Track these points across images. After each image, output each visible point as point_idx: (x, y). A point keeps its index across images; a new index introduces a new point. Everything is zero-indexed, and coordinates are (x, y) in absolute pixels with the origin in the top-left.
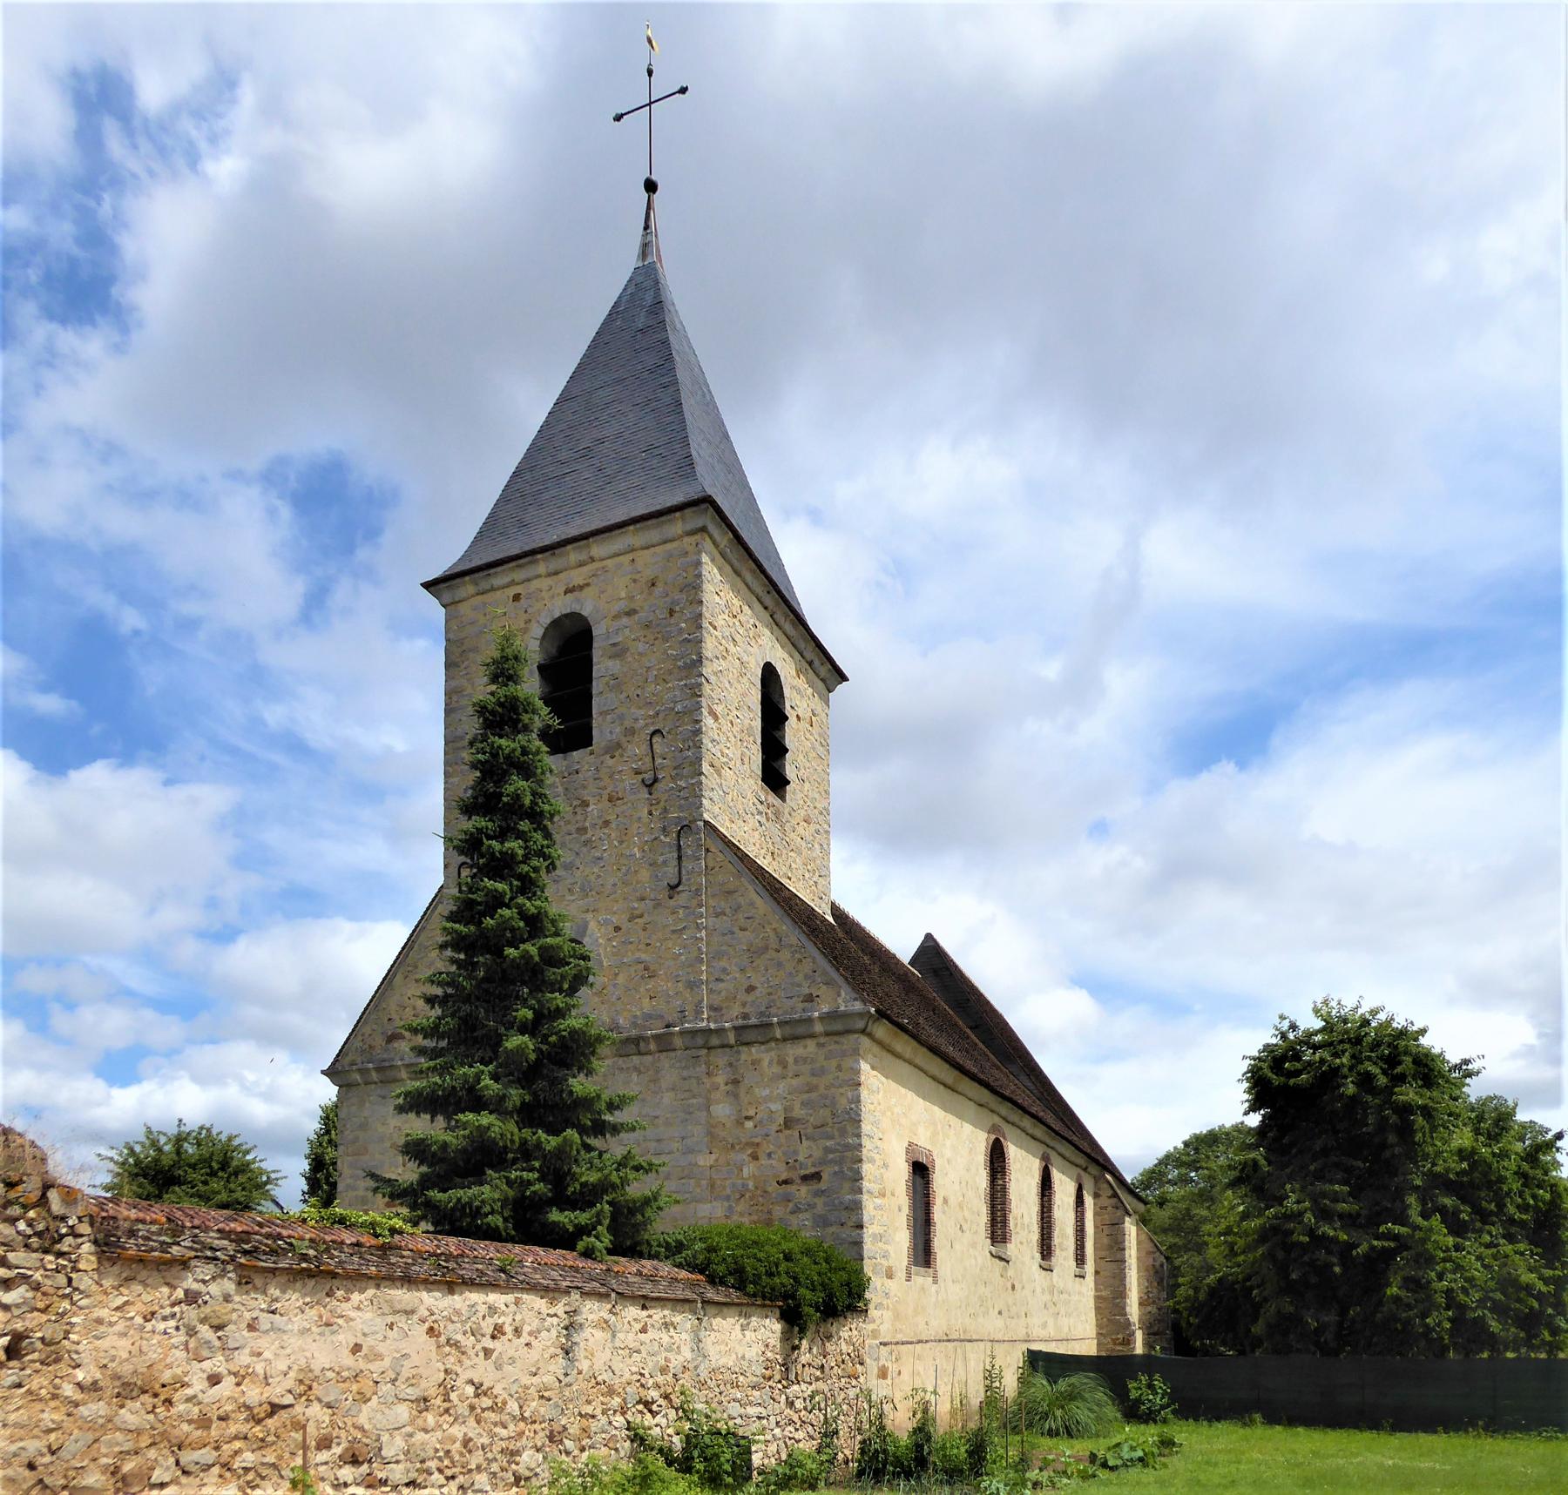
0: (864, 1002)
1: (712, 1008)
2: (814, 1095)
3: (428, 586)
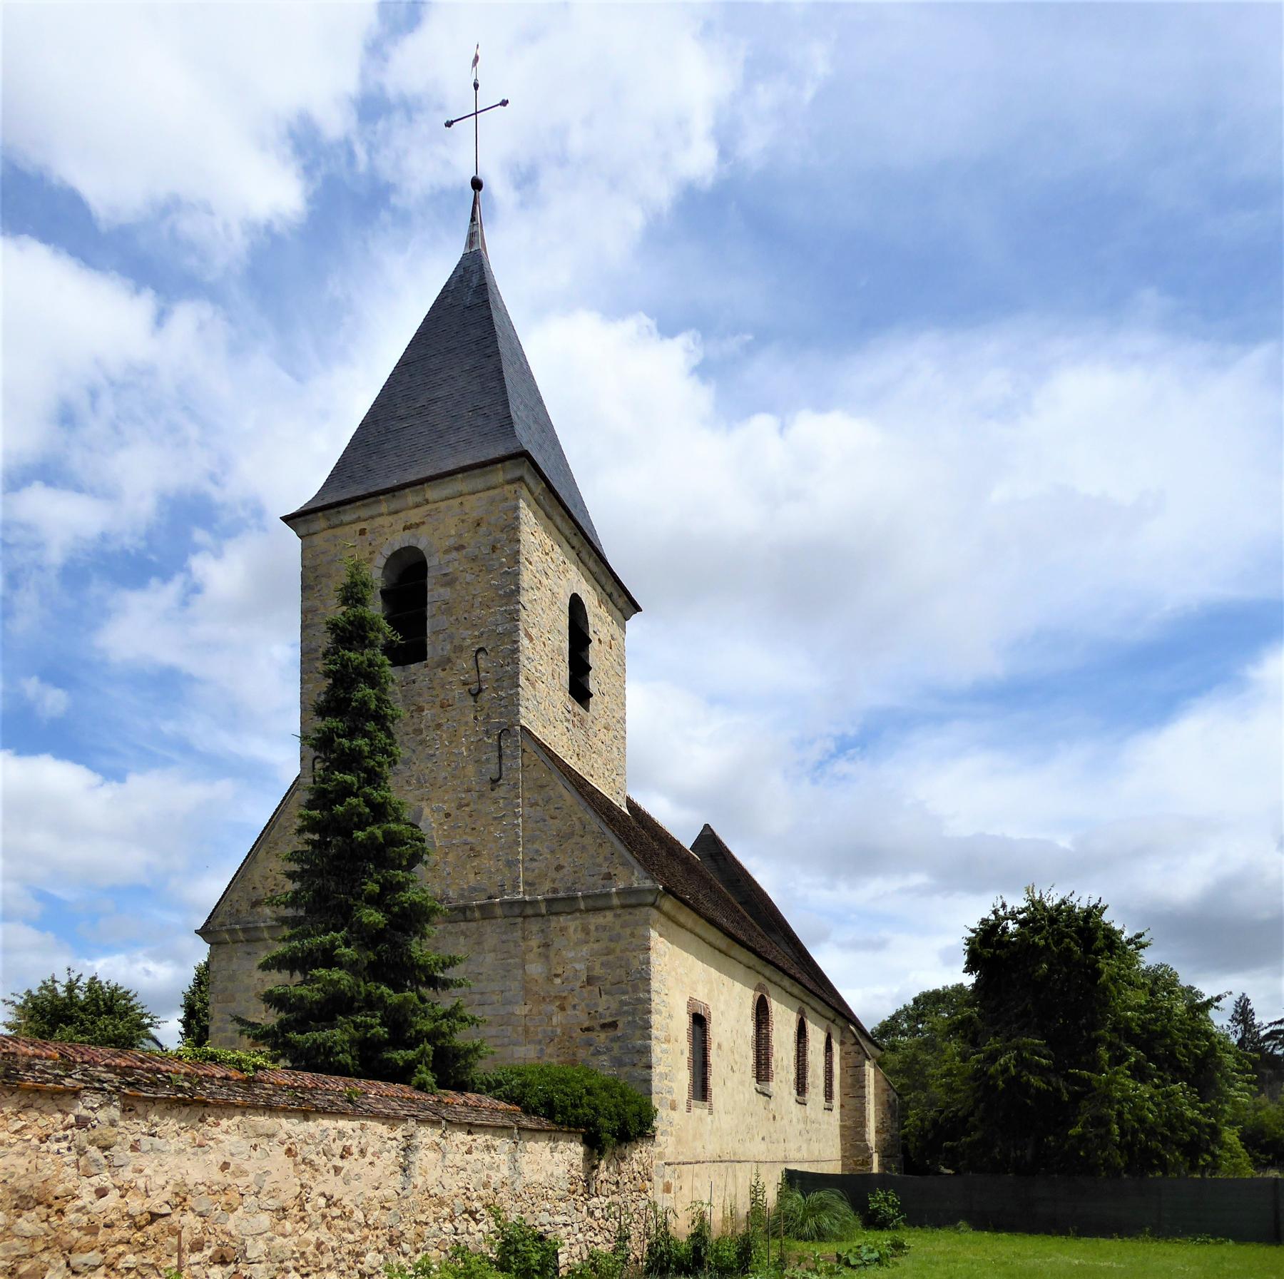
2: (611, 957)
3: (287, 519)
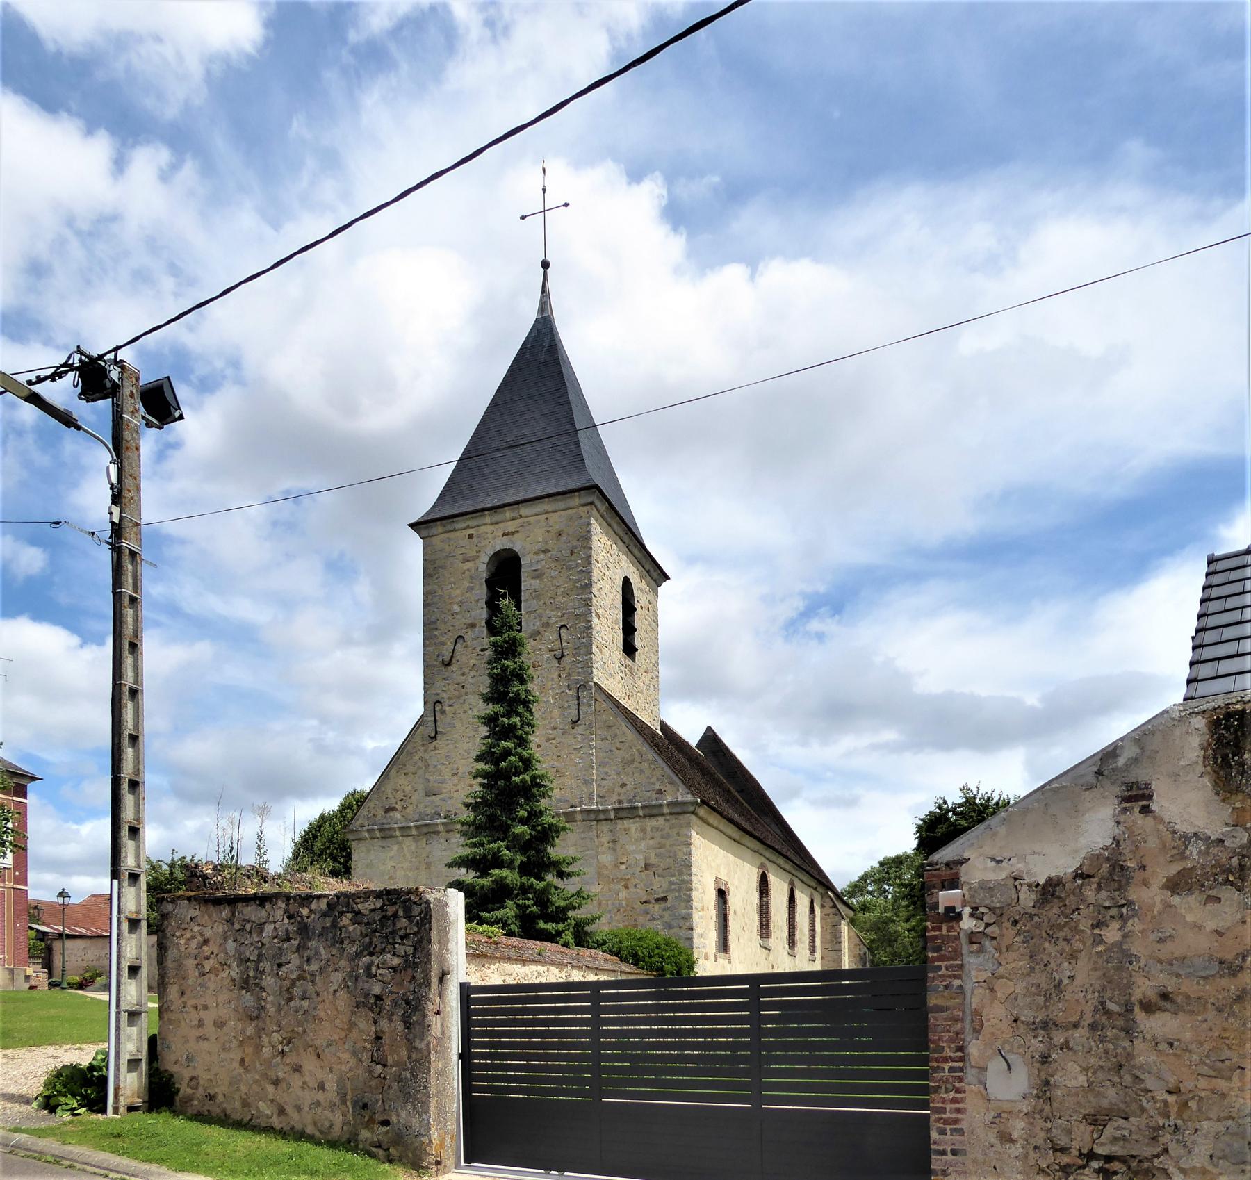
0: (693, 795)
1: (598, 796)
2: (662, 850)
3: (412, 526)
